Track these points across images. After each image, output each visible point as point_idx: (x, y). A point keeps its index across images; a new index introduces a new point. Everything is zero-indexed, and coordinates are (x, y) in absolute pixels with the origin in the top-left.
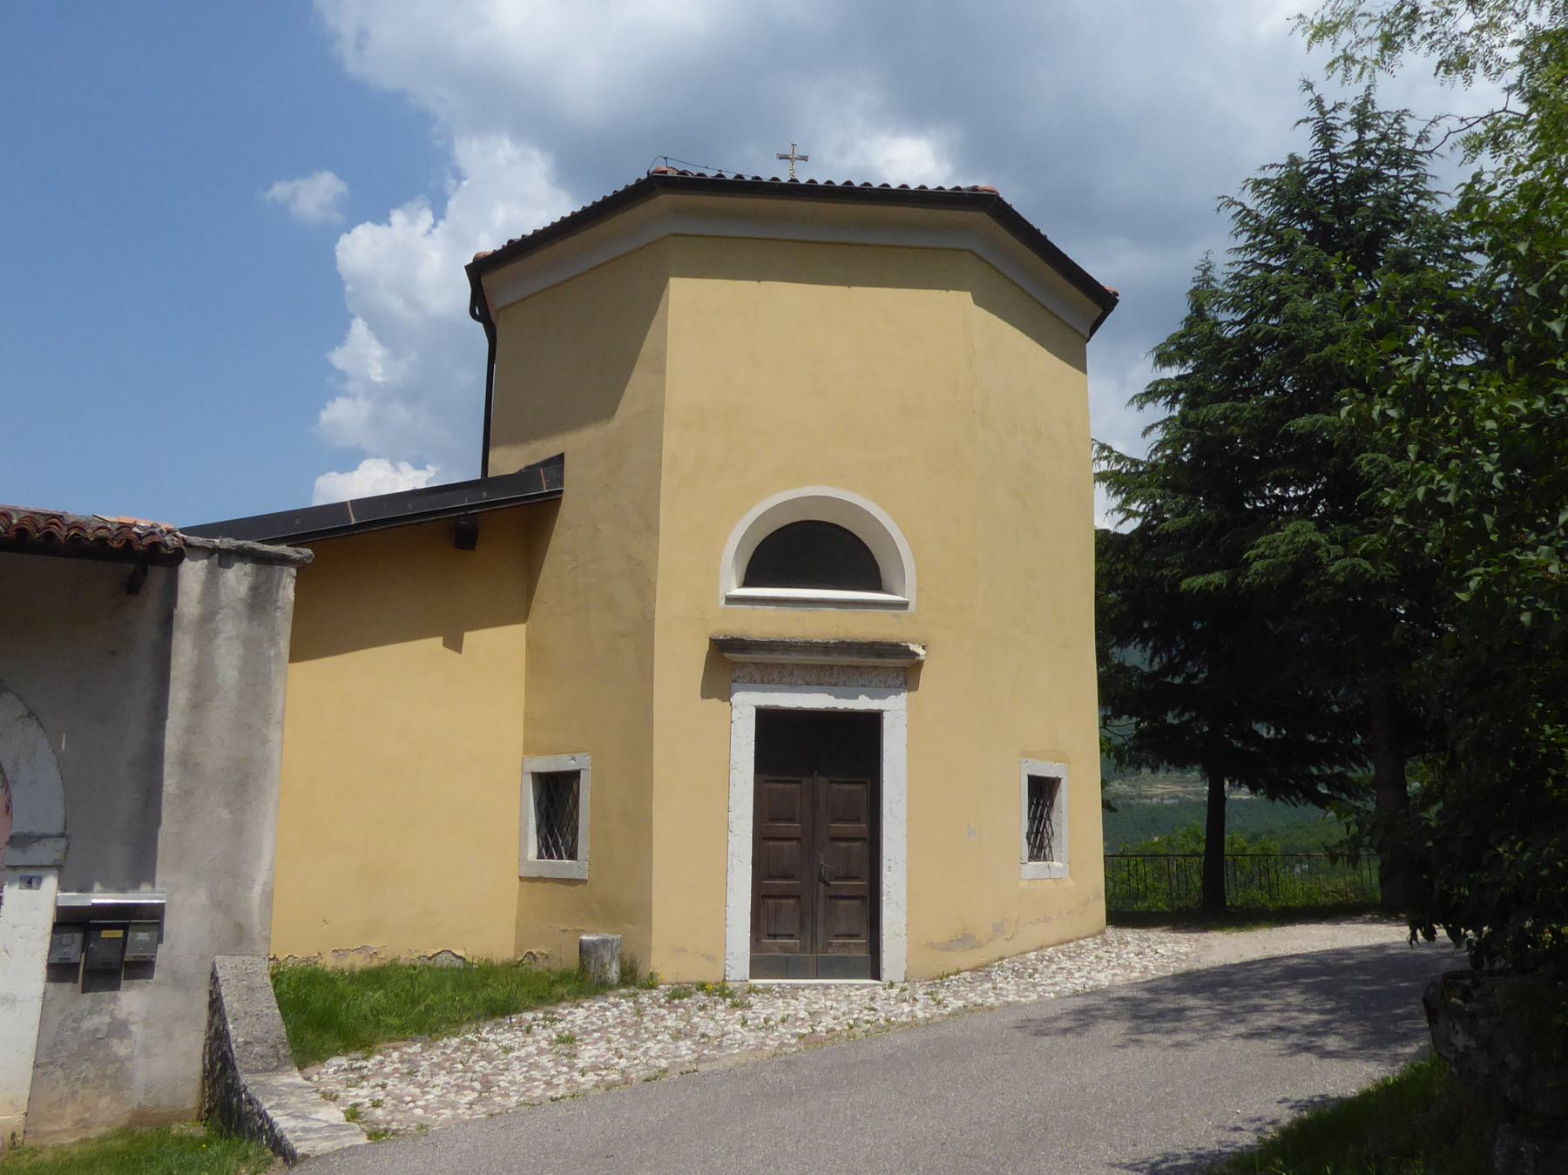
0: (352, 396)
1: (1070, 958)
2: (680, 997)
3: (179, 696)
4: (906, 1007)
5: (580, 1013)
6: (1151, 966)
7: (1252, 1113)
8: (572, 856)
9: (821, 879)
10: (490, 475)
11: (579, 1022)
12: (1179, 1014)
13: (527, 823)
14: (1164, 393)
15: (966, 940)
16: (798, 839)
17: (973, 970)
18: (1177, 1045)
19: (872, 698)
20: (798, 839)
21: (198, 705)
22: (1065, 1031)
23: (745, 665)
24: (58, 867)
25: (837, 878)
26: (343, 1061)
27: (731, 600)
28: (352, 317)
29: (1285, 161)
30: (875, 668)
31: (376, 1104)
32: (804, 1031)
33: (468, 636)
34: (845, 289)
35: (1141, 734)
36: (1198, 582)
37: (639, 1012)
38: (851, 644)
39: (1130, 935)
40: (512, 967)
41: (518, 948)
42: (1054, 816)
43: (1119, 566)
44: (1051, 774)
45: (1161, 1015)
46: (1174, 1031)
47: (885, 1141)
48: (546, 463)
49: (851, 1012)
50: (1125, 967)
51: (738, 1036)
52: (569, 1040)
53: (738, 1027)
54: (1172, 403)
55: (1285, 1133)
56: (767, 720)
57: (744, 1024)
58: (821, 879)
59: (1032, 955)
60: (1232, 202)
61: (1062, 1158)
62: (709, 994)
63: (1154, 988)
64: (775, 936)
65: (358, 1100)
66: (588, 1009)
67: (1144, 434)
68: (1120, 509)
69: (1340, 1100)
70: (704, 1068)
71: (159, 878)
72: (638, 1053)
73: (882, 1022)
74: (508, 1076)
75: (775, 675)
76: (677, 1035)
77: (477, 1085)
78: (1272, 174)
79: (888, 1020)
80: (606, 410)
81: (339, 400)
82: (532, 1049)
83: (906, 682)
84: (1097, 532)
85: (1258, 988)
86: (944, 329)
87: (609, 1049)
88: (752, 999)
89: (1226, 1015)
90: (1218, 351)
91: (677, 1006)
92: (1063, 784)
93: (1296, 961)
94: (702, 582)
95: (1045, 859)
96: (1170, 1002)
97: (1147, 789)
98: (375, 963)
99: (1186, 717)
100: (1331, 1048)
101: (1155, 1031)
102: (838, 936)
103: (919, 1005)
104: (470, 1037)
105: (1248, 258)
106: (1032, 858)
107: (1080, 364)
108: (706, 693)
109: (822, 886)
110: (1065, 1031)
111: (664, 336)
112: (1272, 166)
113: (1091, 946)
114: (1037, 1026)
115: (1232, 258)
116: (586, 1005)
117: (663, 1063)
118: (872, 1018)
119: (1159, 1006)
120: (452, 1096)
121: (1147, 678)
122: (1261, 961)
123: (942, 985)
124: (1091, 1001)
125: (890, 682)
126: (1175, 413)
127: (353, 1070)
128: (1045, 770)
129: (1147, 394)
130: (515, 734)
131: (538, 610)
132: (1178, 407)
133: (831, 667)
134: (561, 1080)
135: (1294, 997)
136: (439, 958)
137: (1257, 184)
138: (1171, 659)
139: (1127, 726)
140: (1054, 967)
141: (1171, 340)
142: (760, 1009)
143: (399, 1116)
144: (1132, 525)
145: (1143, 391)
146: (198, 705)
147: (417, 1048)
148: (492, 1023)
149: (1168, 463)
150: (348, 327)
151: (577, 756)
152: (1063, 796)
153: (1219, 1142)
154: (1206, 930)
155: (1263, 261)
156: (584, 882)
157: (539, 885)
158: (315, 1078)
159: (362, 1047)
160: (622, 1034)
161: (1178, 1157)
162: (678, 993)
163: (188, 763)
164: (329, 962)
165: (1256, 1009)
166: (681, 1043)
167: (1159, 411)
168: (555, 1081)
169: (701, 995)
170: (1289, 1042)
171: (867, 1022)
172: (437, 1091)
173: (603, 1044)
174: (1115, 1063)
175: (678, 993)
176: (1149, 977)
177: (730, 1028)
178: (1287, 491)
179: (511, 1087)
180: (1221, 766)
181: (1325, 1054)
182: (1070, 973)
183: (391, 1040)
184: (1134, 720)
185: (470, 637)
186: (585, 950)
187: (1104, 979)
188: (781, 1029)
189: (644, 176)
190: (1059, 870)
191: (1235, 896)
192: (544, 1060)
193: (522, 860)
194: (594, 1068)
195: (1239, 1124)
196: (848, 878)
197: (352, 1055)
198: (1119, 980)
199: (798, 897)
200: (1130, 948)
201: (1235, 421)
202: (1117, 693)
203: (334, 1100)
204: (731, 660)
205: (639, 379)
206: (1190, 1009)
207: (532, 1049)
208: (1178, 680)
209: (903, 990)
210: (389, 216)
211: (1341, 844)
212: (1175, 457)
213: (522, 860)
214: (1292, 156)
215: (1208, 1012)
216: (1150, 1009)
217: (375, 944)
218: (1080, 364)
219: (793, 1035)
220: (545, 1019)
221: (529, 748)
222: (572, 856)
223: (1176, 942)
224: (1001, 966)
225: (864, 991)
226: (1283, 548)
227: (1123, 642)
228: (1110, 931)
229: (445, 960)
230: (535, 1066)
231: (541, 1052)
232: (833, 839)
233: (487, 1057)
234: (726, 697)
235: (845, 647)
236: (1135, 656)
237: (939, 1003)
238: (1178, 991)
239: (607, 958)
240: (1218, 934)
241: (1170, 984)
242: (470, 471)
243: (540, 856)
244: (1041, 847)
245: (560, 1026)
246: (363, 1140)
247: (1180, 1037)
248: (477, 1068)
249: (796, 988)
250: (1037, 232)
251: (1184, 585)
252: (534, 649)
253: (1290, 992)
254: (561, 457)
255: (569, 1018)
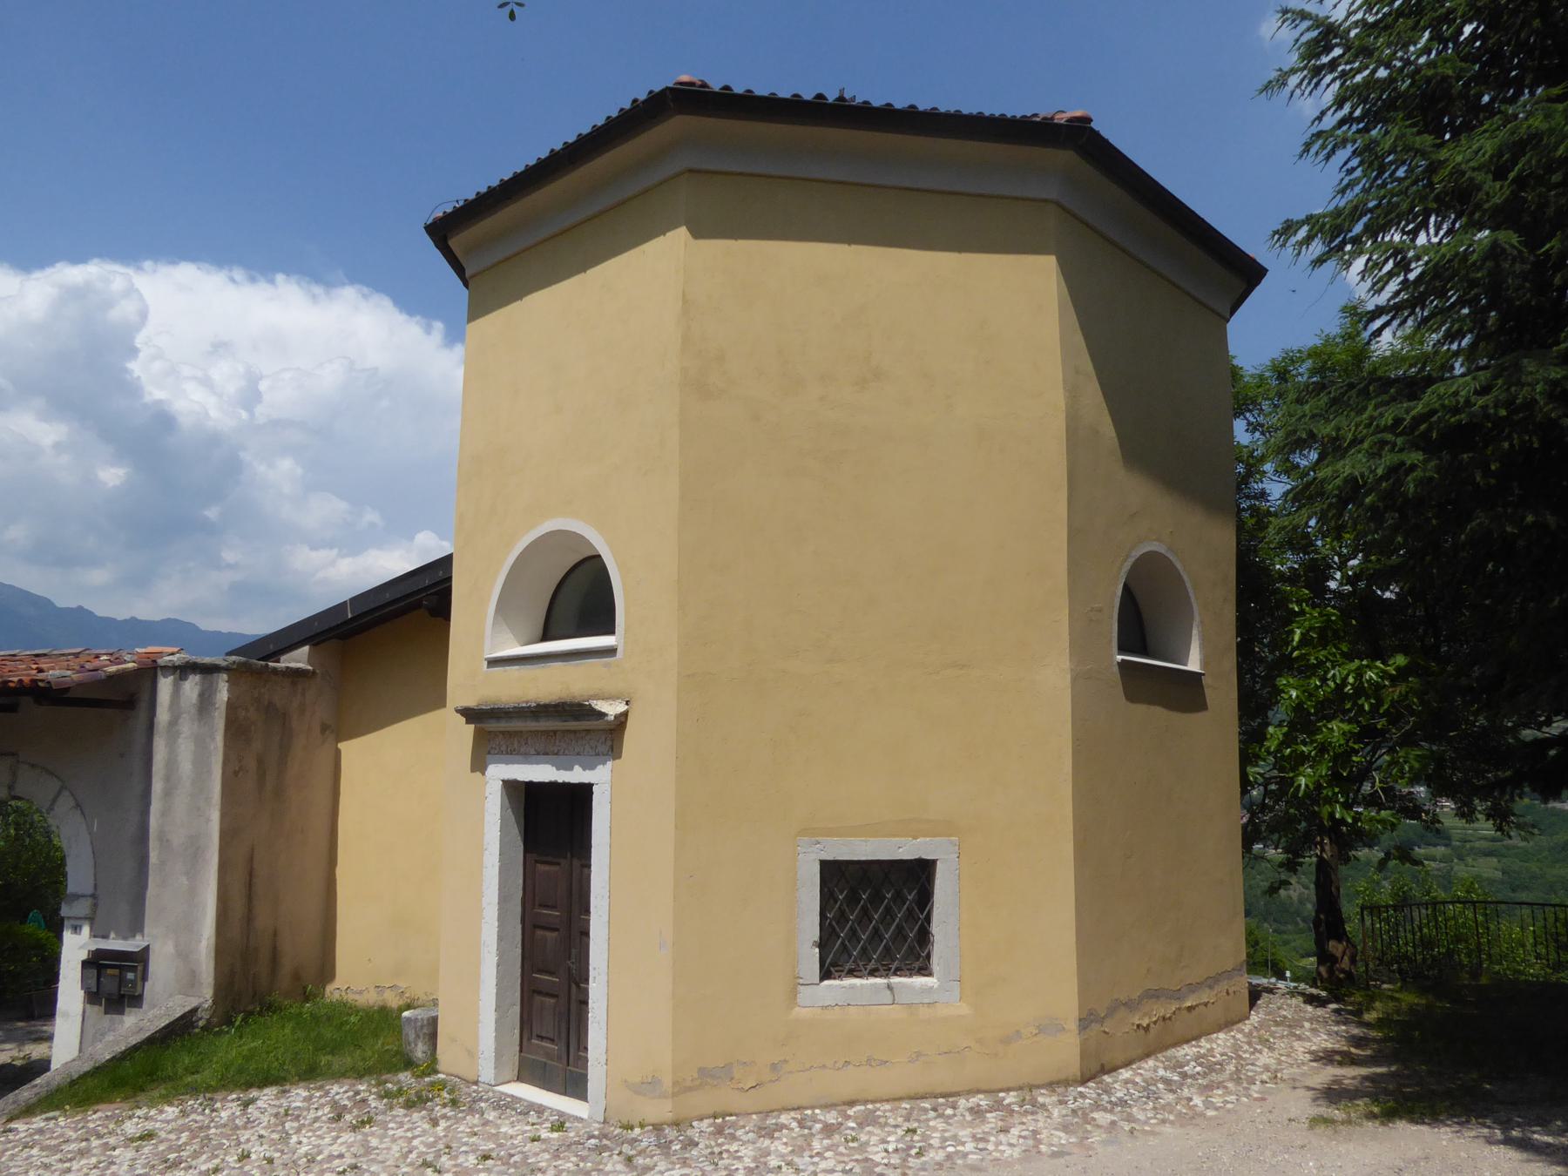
3: (157, 786)
21: (168, 793)
24: (91, 919)
38: (546, 706)
71: (146, 930)
87: (249, 1123)
108: (473, 770)
133: (555, 732)
146: (168, 793)
163: (164, 841)
217: (403, 985)
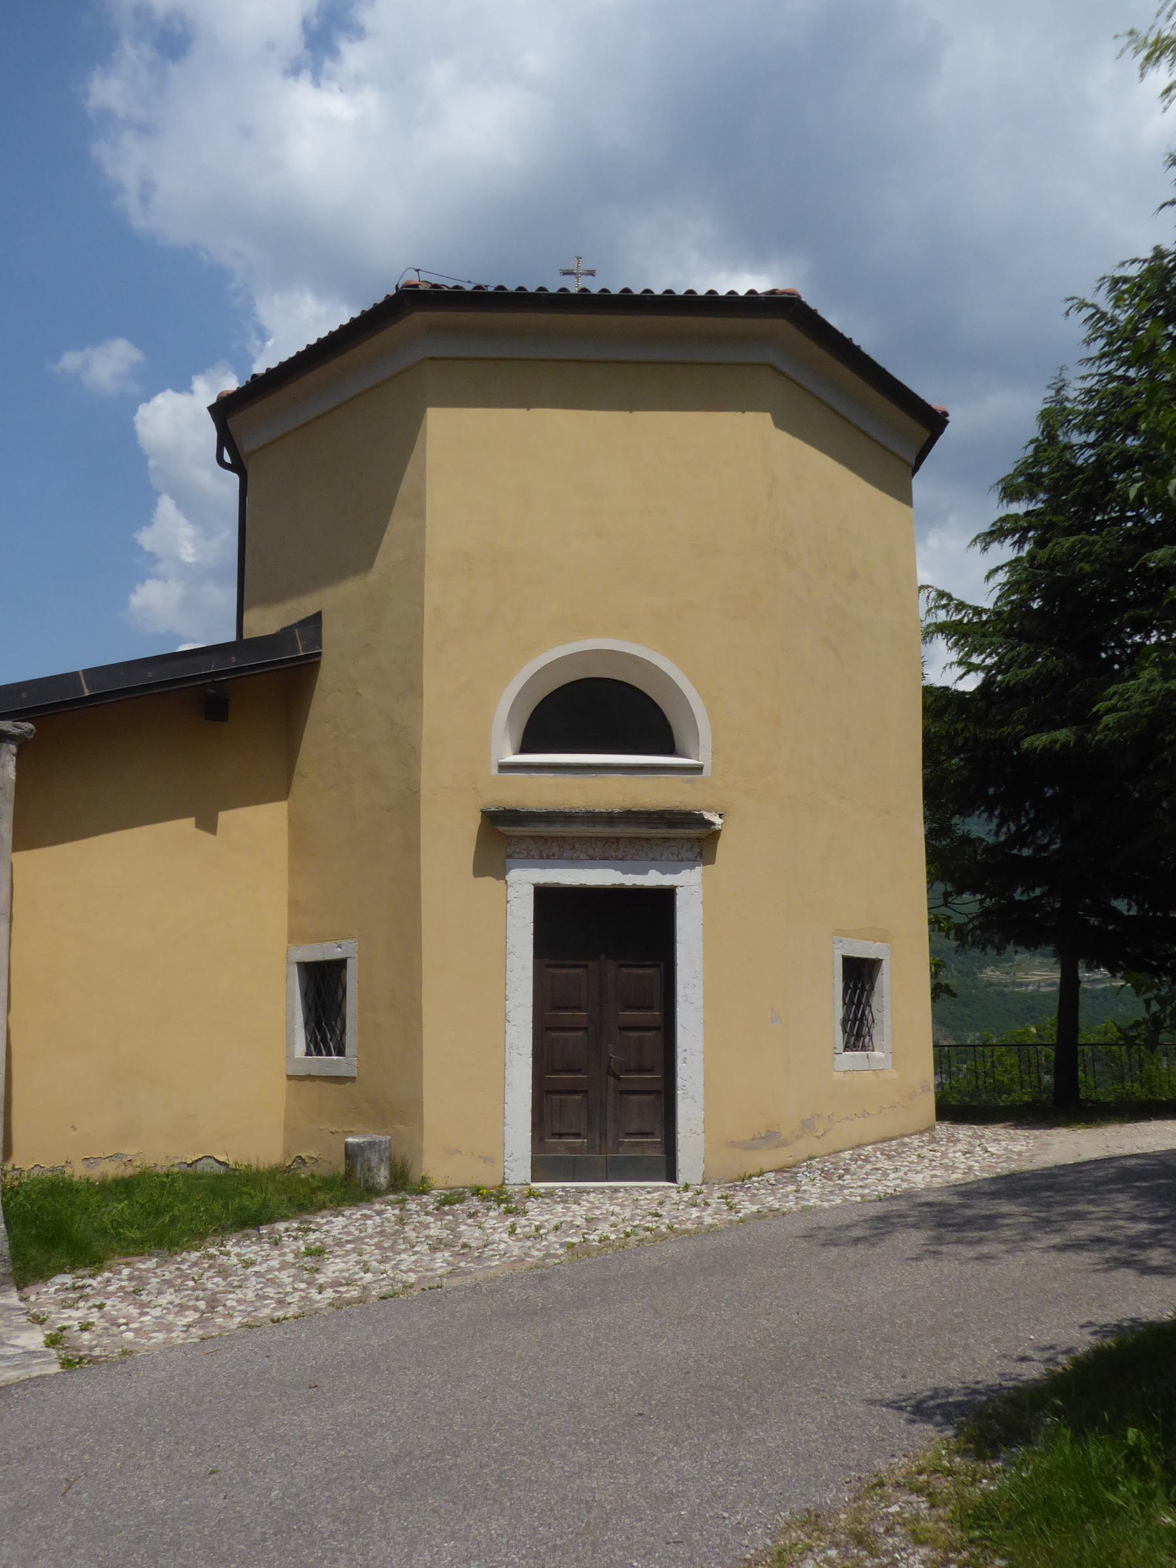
0: (163, 578)
1: (889, 1157)
2: (451, 1204)
4: (695, 1213)
5: (340, 1221)
6: (976, 1166)
7: (1047, 1340)
8: (341, 1052)
9: (610, 1072)
10: (245, 637)
11: (335, 1232)
12: (990, 1222)
13: (293, 1015)
14: (1012, 532)
15: (770, 1138)
16: (585, 1029)
17: (776, 1171)
18: (981, 1258)
19: (664, 873)
20: (585, 1029)
22: (857, 1241)
23: (521, 838)
25: (628, 1071)
26: (67, 1279)
27: (505, 768)
28: (159, 494)
29: (1149, 255)
30: (666, 839)
31: (85, 1328)
32: (575, 1240)
33: (223, 816)
34: (626, 414)
35: (985, 913)
36: (1040, 740)
37: (401, 1221)
39: (964, 1132)
40: (274, 1172)
41: (287, 1152)
42: (875, 1001)
43: (959, 726)
44: (872, 955)
45: (970, 1223)
46: (980, 1241)
47: (623, 1369)
48: (303, 623)
49: (633, 1218)
50: (946, 1167)
51: (503, 1246)
52: (317, 1253)
53: (505, 1236)
54: (1020, 543)
55: (1077, 1363)
56: (545, 897)
57: (512, 1231)
58: (610, 1072)
59: (847, 1155)
60: (1083, 305)
61: (817, 1391)
62: (485, 1198)
63: (969, 1192)
64: (560, 1135)
65: (66, 1324)
66: (349, 1218)
67: (988, 578)
68: (960, 663)
69: (1150, 1325)
70: (455, 1282)
72: (388, 1266)
73: (663, 1229)
74: (239, 1294)
75: (555, 849)
76: (437, 1246)
77: (202, 1305)
78: (1133, 271)
79: (670, 1228)
80: (363, 560)
81: (149, 582)
82: (275, 1263)
83: (701, 854)
84: (928, 691)
85: (1086, 1191)
86: (742, 459)
88: (529, 1205)
89: (1043, 1224)
90: (1067, 478)
91: (446, 1214)
92: (885, 967)
93: (1133, 1162)
94: (473, 747)
95: (864, 1048)
96: (984, 1207)
97: (1021, 976)
98: (129, 1171)
99: (1038, 892)
100: (1155, 1263)
101: (959, 1242)
102: (629, 1135)
103: (710, 1210)
104: (212, 1250)
105: (1103, 370)
106: (847, 1048)
107: (904, 496)
109: (611, 1079)
110: (857, 1241)
111: (422, 476)
112: (1134, 261)
113: (916, 1143)
114: (829, 1235)
115: (1085, 370)
116: (347, 1213)
117: (412, 1278)
118: (654, 1226)
119: (968, 1212)
120: (170, 1318)
121: (992, 850)
122: (1096, 1161)
123: (742, 1187)
124: (894, 1207)
125: (684, 855)
126: (1023, 554)
127: (75, 1289)
128: (863, 950)
129: (991, 533)
130: (277, 919)
131: (299, 786)
132: (1027, 547)
133: (618, 839)
134: (294, 1298)
135: (1124, 1203)
136: (200, 1166)
137: (1116, 281)
138: (1020, 828)
139: (969, 904)
140: (869, 1167)
141: (1018, 472)
142: (536, 1214)
143: (106, 1341)
144: (971, 683)
145: (986, 529)
147: (151, 1263)
148: (239, 1235)
149: (1012, 610)
150: (154, 504)
151: (343, 943)
152: (885, 980)
153: (1002, 1375)
154: (1051, 1127)
155: (1120, 372)
156: (353, 1079)
157: (307, 1083)
158: (33, 1298)
159: (92, 1263)
160: (378, 1246)
161: (949, 1392)
162: (451, 1199)
164: (78, 1171)
165: (1078, 1216)
166: (439, 1255)
167: (1004, 551)
168: (289, 1299)
169: (475, 1203)
170: (1107, 1255)
171: (648, 1229)
172: (157, 1312)
173: (354, 1257)
174: (904, 1277)
175: (451, 1199)
176: (971, 1178)
177: (496, 1237)
178: (1148, 637)
179: (240, 1304)
180: (1076, 943)
181: (1147, 1270)
182: (885, 1175)
183: (126, 1255)
184: (979, 897)
185: (225, 817)
186: (351, 1154)
187: (920, 1181)
188: (552, 1238)
189: (392, 292)
190: (880, 1060)
191: (1093, 1083)
192: (284, 1277)
193: (290, 1056)
194: (335, 1284)
195: (1030, 1353)
196: (639, 1070)
197: (80, 1272)
198: (937, 1183)
199: (585, 1092)
200: (959, 1146)
201: (1086, 557)
202: (948, 863)
203: (42, 1322)
204: (507, 833)
205: (398, 523)
206: (1003, 1216)
207: (275, 1263)
208: (1026, 852)
209: (699, 1193)
210: (190, 383)
211: (1137, 1024)
212: (1024, 603)
213: (290, 1056)
214: (1157, 249)
215: (1024, 1219)
216: (955, 1218)
217: (129, 1151)
218: (904, 496)
219: (562, 1245)
220: (299, 1229)
221: (295, 936)
222: (341, 1052)
223: (1013, 1140)
224: (809, 1167)
225: (656, 1195)
226: (1137, 698)
227: (966, 810)
228: (943, 1129)
229: (206, 1167)
230: (272, 1282)
231: (284, 1266)
232: (622, 1029)
233: (224, 1272)
234: (501, 874)
235: (631, 817)
236: (979, 827)
237: (731, 1208)
238: (994, 1195)
239: (375, 1160)
240: (1063, 1131)
241: (986, 1189)
242: (230, 636)
243: (308, 1053)
244: (859, 1036)
245: (312, 1236)
246: (55, 1368)
247: (985, 1249)
248: (209, 1285)
249: (580, 1191)
250: (848, 342)
251: (1026, 744)
252: (296, 826)
253: (1121, 1197)
254: (318, 616)
255: (326, 1228)
